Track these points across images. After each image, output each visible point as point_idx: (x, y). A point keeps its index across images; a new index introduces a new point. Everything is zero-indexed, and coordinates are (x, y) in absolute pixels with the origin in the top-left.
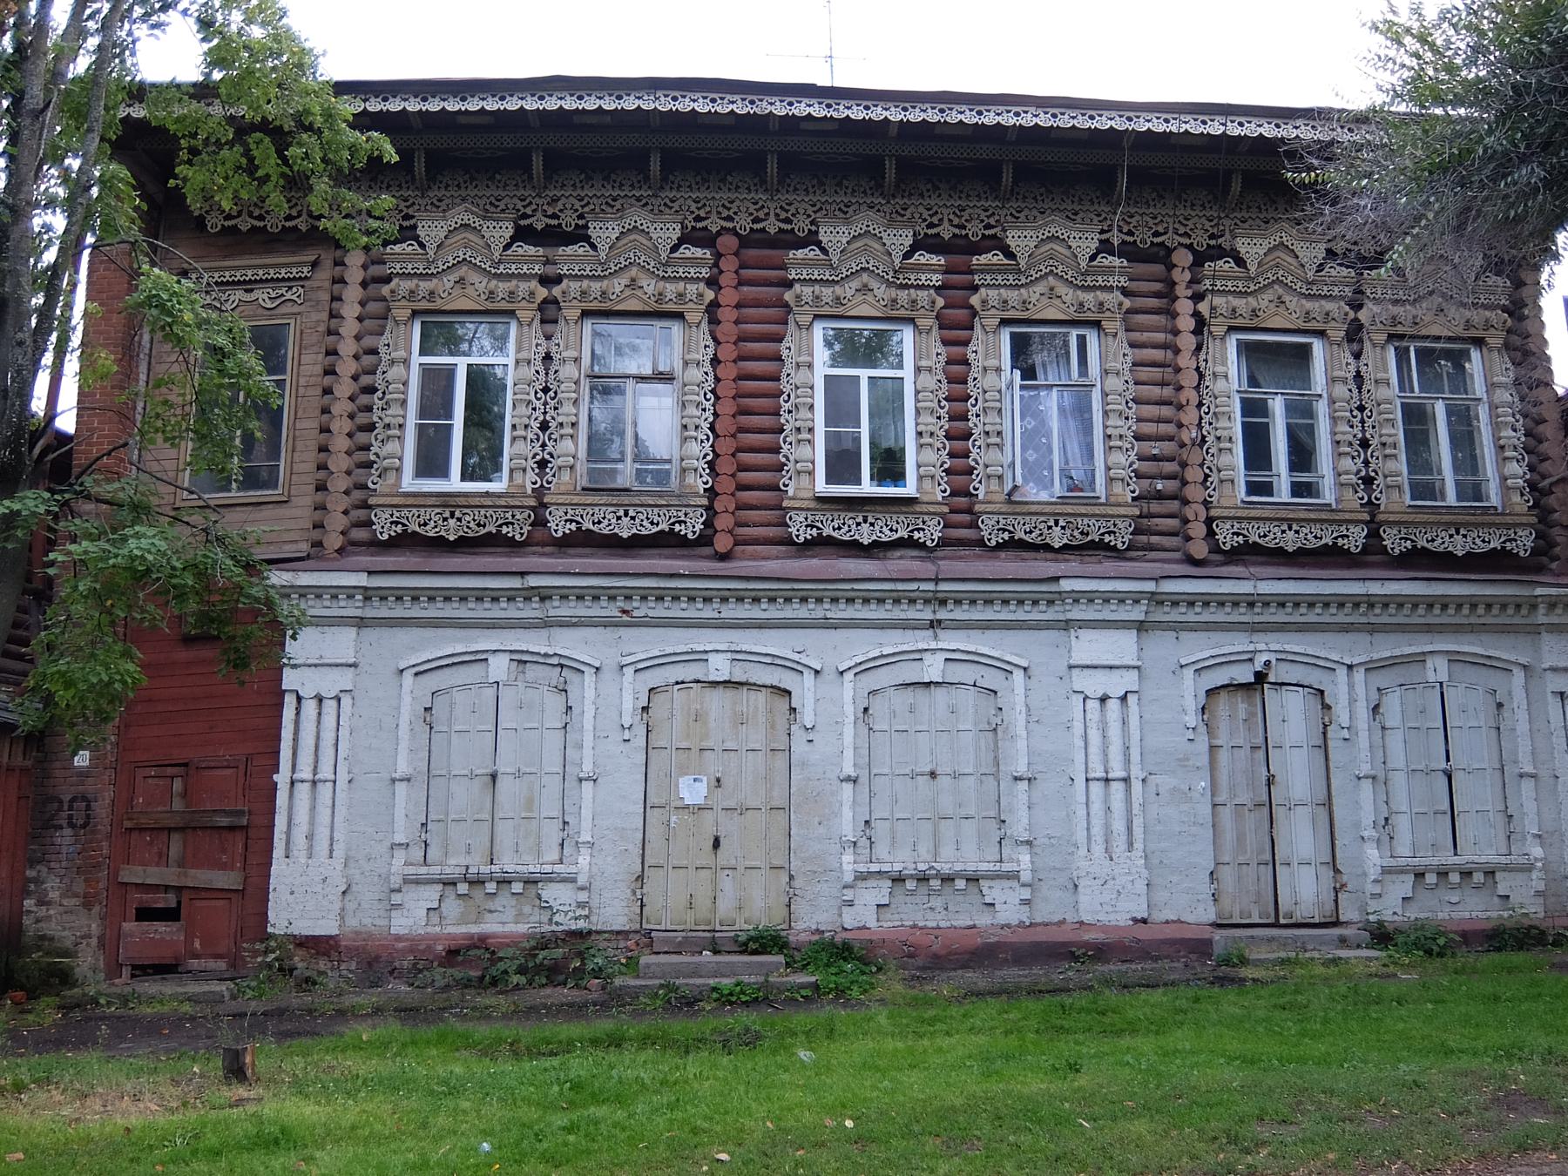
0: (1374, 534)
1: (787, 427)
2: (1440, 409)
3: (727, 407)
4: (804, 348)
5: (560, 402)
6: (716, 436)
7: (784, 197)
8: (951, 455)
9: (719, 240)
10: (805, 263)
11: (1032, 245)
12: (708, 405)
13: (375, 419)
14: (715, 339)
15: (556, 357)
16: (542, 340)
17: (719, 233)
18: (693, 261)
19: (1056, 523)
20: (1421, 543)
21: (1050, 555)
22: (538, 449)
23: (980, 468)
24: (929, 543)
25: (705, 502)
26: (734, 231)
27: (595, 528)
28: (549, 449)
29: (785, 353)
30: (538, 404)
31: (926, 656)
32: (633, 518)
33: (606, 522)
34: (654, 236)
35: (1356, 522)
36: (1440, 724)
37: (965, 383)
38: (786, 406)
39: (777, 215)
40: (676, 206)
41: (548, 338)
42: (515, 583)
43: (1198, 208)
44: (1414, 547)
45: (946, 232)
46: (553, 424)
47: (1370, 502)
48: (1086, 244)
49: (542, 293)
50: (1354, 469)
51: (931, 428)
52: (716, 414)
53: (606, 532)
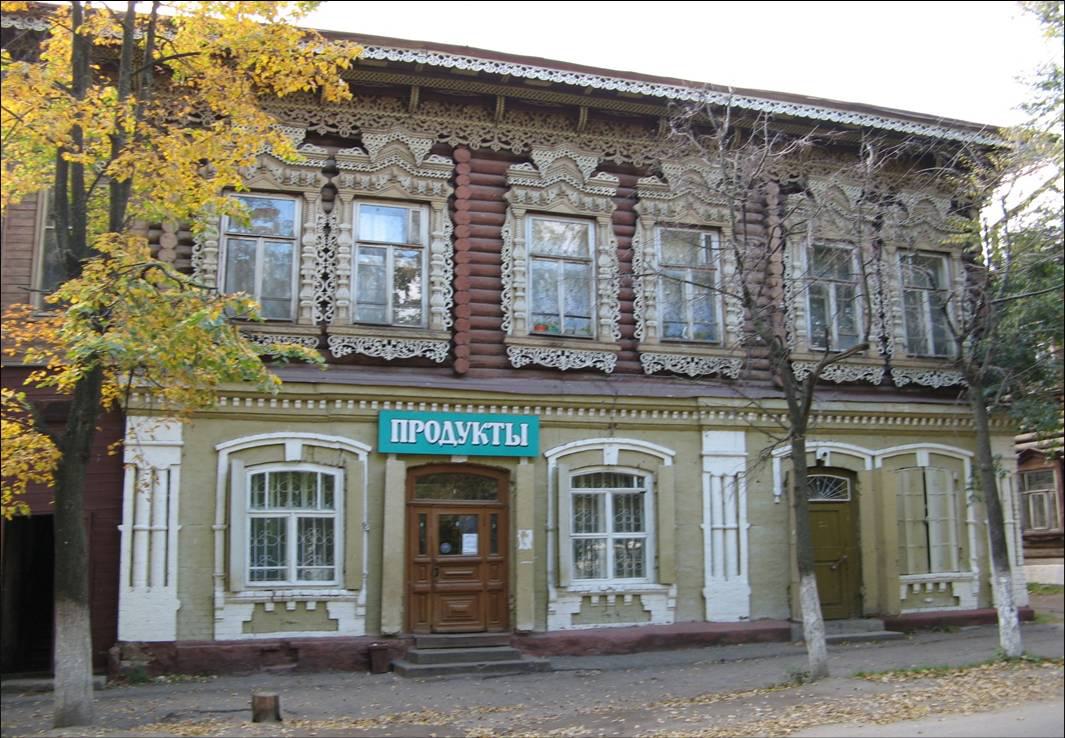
0: (888, 373)
1: (507, 287)
2: (832, 292)
3: (462, 270)
4: (519, 233)
5: (338, 260)
6: (455, 291)
7: (505, 127)
8: (622, 311)
9: (456, 152)
10: (521, 174)
11: (550, 161)
12: (449, 268)
13: (193, 265)
14: (453, 220)
15: (333, 227)
16: (323, 215)
17: (456, 148)
18: (438, 167)
19: (693, 360)
20: (915, 380)
21: (686, 382)
22: (320, 294)
23: (641, 322)
24: (607, 371)
25: (449, 337)
26: (467, 147)
27: (366, 353)
28: (329, 293)
29: (504, 235)
30: (321, 261)
31: (605, 447)
32: (394, 346)
33: (549, 359)
34: (412, 147)
35: (878, 365)
36: (922, 493)
37: (499, 252)
38: (506, 272)
39: (499, 139)
40: (426, 126)
41: (328, 212)
42: (309, 390)
43: (301, 102)
44: (354, 352)
45: (618, 160)
46: (331, 276)
47: (885, 353)
48: (589, 163)
49: (325, 180)
50: (737, 322)
51: (312, 272)
52: (455, 276)
53: (374, 355)
